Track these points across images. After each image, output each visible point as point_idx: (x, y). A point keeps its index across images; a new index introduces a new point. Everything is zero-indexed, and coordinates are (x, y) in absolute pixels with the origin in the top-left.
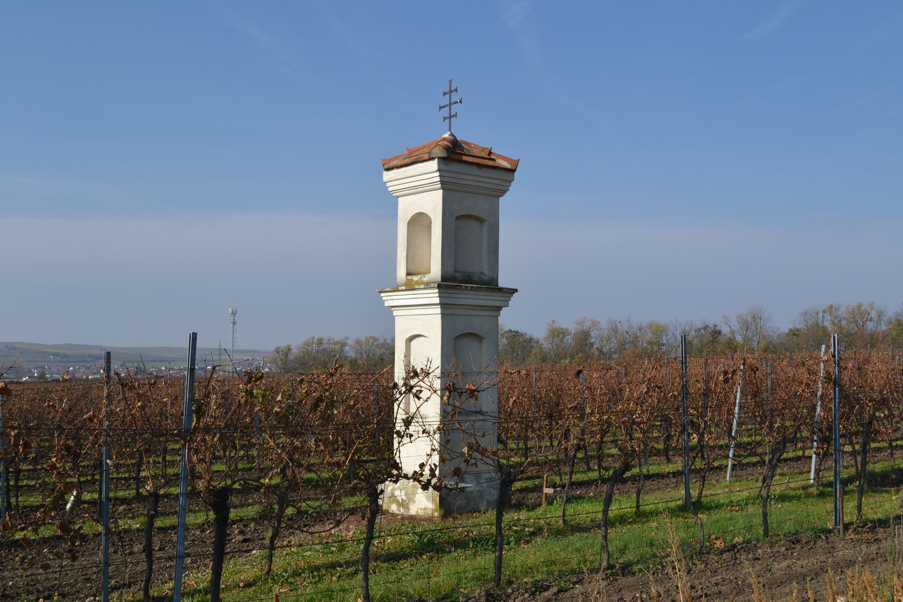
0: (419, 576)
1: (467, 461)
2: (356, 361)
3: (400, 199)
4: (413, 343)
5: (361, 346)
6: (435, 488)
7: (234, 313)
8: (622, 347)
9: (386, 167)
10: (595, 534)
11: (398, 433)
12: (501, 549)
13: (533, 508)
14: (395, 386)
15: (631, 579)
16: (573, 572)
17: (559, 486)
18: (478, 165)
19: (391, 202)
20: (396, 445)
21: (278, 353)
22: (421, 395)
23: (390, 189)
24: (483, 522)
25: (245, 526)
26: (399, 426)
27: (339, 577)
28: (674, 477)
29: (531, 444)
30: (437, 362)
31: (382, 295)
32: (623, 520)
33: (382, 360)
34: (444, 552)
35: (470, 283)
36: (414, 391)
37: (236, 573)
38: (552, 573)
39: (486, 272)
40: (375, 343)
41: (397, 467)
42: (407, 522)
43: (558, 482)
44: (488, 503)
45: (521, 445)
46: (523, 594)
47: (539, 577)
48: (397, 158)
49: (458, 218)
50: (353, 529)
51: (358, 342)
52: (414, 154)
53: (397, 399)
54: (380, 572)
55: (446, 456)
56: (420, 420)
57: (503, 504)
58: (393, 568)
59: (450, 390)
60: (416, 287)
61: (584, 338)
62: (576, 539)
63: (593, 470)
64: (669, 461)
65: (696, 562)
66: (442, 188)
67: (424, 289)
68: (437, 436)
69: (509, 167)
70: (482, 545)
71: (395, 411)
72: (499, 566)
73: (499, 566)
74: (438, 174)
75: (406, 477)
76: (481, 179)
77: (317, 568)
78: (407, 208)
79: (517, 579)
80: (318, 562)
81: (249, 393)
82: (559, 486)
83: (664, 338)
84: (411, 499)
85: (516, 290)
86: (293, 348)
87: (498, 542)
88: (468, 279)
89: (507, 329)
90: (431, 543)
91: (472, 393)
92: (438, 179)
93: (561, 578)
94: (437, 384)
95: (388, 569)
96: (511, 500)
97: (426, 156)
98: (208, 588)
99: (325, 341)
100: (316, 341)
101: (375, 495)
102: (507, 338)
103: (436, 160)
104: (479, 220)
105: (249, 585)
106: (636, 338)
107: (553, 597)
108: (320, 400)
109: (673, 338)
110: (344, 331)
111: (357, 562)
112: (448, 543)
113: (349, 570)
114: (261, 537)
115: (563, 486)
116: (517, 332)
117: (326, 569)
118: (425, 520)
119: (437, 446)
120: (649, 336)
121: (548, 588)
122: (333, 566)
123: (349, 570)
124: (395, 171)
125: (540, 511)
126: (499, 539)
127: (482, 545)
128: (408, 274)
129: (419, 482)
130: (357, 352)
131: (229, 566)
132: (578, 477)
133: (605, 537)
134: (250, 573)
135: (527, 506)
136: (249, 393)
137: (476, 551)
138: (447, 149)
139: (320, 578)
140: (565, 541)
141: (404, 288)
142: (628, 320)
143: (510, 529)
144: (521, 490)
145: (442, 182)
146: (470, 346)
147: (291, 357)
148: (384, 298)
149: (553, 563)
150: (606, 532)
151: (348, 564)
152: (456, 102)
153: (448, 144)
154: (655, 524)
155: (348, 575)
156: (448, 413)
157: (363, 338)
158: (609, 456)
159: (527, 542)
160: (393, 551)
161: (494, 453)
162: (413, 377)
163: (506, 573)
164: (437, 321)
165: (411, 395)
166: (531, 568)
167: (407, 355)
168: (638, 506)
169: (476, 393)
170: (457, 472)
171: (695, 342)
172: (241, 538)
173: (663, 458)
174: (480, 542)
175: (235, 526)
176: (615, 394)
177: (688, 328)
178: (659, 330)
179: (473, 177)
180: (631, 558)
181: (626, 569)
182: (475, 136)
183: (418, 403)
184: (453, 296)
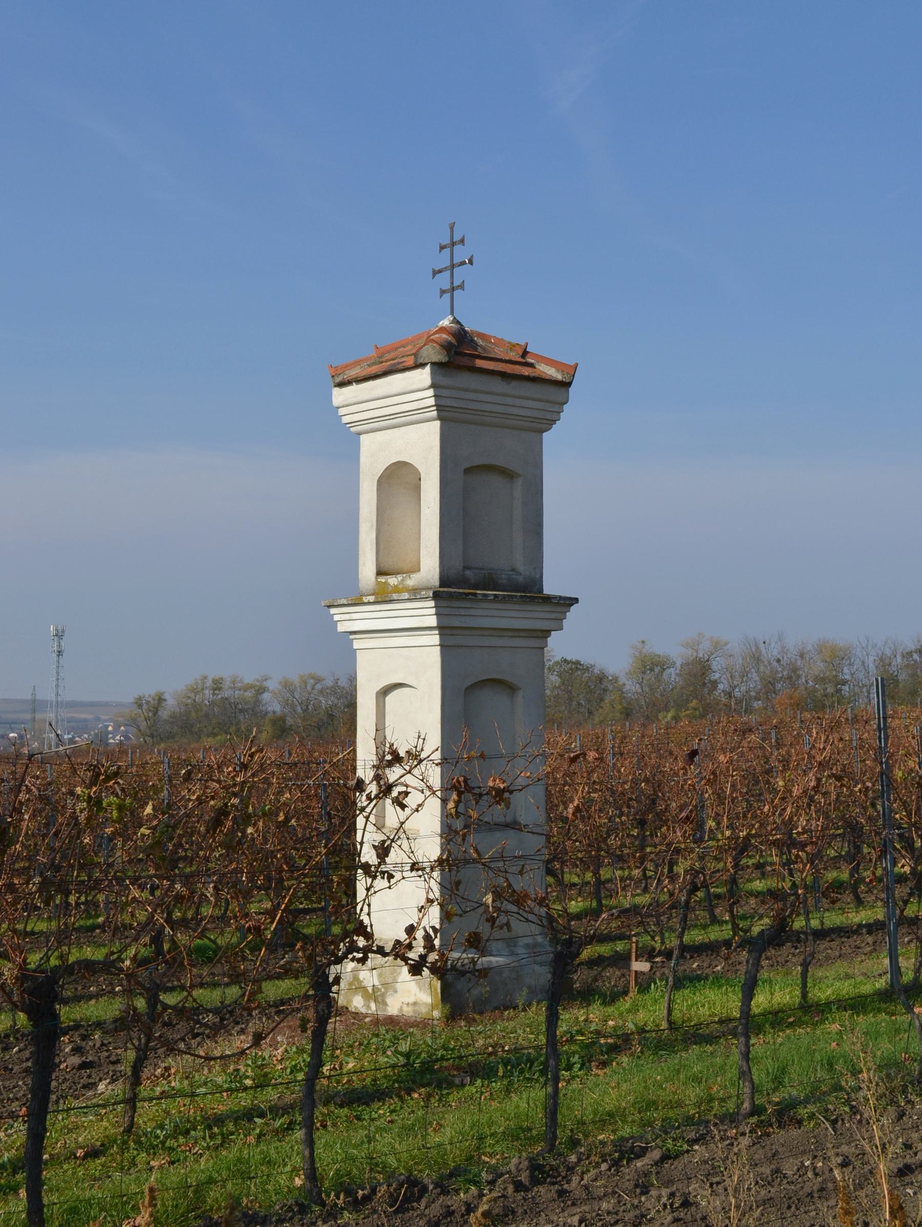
0: (408, 1130)
1: (492, 920)
2: (283, 719)
3: (363, 438)
4: (390, 699)
5: (292, 692)
6: (434, 970)
7: (59, 635)
8: (769, 686)
9: (338, 379)
10: (728, 1047)
11: (366, 867)
12: (556, 1079)
13: (612, 998)
14: (360, 785)
15: (794, 1132)
16: (689, 1121)
17: (660, 953)
18: (504, 375)
19: (347, 442)
20: (361, 893)
21: (140, 706)
22: (406, 801)
23: (345, 420)
24: (523, 1028)
25: (84, 1038)
26: (368, 856)
27: (260, 1136)
28: (870, 933)
29: (605, 873)
30: (434, 740)
31: (333, 611)
32: (777, 1018)
33: (331, 716)
34: (451, 1085)
35: (490, 589)
36: (395, 794)
37: (70, 1131)
38: (650, 1124)
39: (520, 567)
40: (318, 686)
41: (362, 930)
42: (382, 1030)
43: (658, 946)
44: (532, 991)
45: (589, 876)
46: (598, 1165)
47: (626, 1131)
48: (357, 363)
49: (468, 471)
50: (284, 1050)
51: (287, 685)
52: (387, 356)
53: (363, 809)
54: (334, 1125)
55: (452, 908)
56: (405, 842)
57: (559, 994)
58: (359, 1118)
59: (460, 791)
60: (395, 596)
61: (699, 672)
62: (693, 1057)
63: (721, 923)
64: (859, 902)
65: (913, 1098)
66: (440, 418)
67: (409, 600)
68: (436, 874)
69: (559, 377)
70: (522, 1072)
71: (359, 839)
72: (552, 1109)
73: (552, 1109)
74: (431, 392)
75: (381, 951)
76: (510, 401)
77: (219, 1120)
78: (376, 453)
79: (586, 1136)
80: (221, 1109)
81: (95, 803)
82: (660, 953)
83: (846, 670)
84: (389, 986)
85: (576, 600)
86: (166, 696)
87: (549, 1063)
88: (489, 582)
89: (558, 658)
90: (427, 1067)
91: (500, 795)
92: (432, 401)
93: (666, 1133)
94: (435, 776)
95: (348, 1120)
96: (572, 982)
97: (410, 361)
98: (19, 1159)
99: (227, 684)
100: (209, 683)
101: (323, 988)
102: (560, 675)
103: (428, 368)
104: (507, 474)
105: (93, 1153)
106: (795, 670)
107: (654, 1170)
108: (223, 812)
109: (863, 672)
110: (262, 664)
111: (292, 1106)
112: (458, 1068)
113: (278, 1123)
114: (113, 1058)
115: (668, 954)
116: (578, 663)
117: (236, 1120)
118: (415, 1024)
119: (436, 893)
120: (819, 667)
121: (643, 1152)
122: (249, 1114)
123: (278, 1123)
124: (354, 387)
125: (625, 1004)
126: (552, 1062)
127: (522, 1072)
128: (380, 573)
129: (405, 960)
130: (286, 703)
131: (56, 1122)
132: (695, 936)
133: (746, 1056)
134: (96, 1128)
135: (603, 996)
136: (95, 803)
137: (511, 1083)
138: (447, 347)
139: (225, 1137)
140: (675, 1060)
141: (372, 599)
142: (780, 640)
143: (571, 1040)
144: (593, 963)
145: (439, 407)
146: (493, 700)
147: (164, 714)
148: (336, 618)
149: (652, 1104)
150: (747, 1046)
151: (276, 1111)
152: (463, 263)
153: (450, 338)
154: (836, 1027)
155: (277, 1132)
156: (456, 832)
157: (294, 676)
158: (751, 894)
159: (604, 1064)
160: (357, 1084)
161: (542, 902)
162: (390, 764)
163: (567, 1119)
164: (434, 657)
165: (388, 801)
166: (611, 1115)
167: (380, 728)
168: (804, 995)
169: (506, 795)
170: (474, 942)
171: (902, 677)
172: (75, 1060)
173: (848, 897)
174: (515, 1065)
175: (65, 1039)
176: (757, 783)
177: (888, 652)
178: (837, 656)
179: (494, 397)
180: (795, 1093)
181: (786, 1114)
182: (498, 322)
183: (402, 815)
184: (463, 612)
